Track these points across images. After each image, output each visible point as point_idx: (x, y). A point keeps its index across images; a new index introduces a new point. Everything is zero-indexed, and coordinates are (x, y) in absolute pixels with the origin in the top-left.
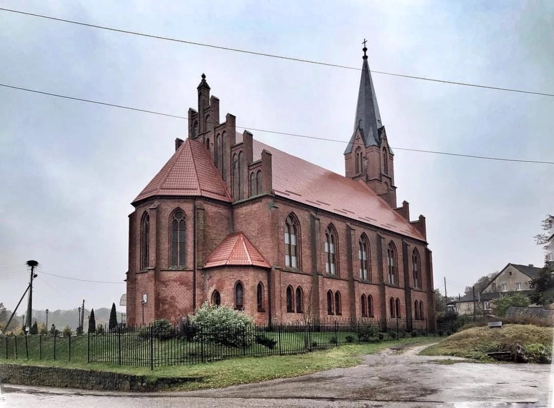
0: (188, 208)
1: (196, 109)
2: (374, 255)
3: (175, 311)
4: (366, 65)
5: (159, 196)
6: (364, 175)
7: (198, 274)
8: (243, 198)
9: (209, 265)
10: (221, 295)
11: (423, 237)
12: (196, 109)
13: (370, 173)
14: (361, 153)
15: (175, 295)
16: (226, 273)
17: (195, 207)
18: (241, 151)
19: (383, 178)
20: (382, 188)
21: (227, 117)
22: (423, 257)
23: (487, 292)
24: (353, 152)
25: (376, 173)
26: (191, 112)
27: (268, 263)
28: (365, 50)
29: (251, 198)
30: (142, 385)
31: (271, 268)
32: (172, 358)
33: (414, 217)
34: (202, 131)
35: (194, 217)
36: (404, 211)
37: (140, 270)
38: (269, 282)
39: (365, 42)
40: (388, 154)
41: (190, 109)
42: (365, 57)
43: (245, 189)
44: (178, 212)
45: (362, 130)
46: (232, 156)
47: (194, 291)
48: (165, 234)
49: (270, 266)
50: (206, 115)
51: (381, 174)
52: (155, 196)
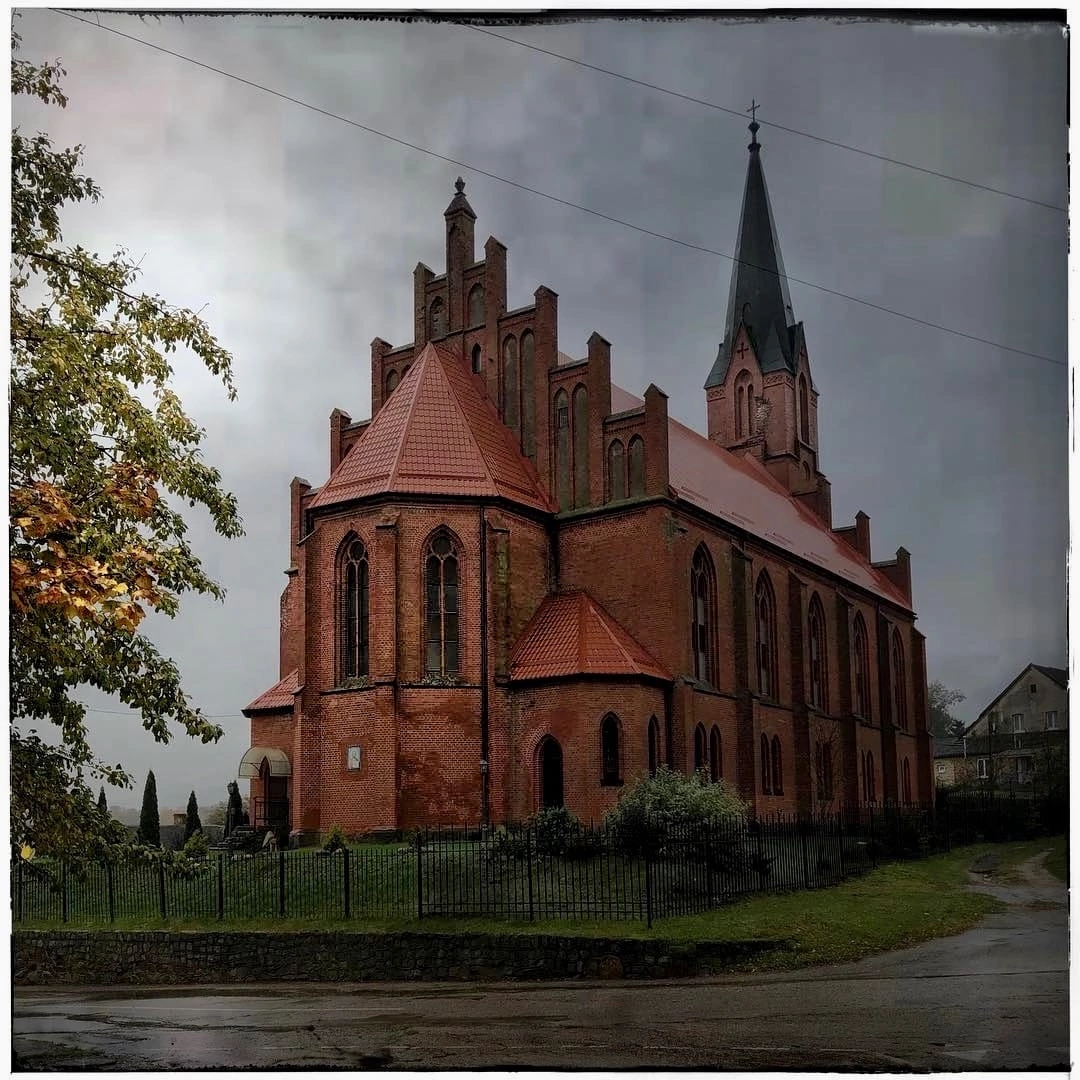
0: (465, 526)
1: (440, 270)
2: (832, 647)
3: (438, 789)
4: (755, 168)
5: (396, 494)
6: (756, 444)
7: (497, 696)
8: (589, 504)
9: (520, 675)
10: (563, 748)
11: (907, 601)
12: (440, 270)
13: (773, 439)
14: (751, 388)
15: (439, 751)
16: (581, 694)
17: (484, 524)
18: (580, 385)
19: (803, 452)
20: (797, 474)
21: (537, 294)
22: (908, 646)
23: (978, 733)
24: (731, 382)
25: (788, 440)
26: (423, 275)
27: (662, 667)
28: (754, 128)
29: (611, 505)
30: (656, 963)
31: (673, 683)
32: (547, 912)
33: (882, 551)
34: (458, 323)
35: (483, 550)
36: (855, 539)
37: (335, 686)
38: (669, 716)
39: (754, 109)
40: (809, 392)
41: (420, 264)
42: (754, 147)
43: (598, 481)
44: (442, 537)
45: (751, 327)
46: (552, 399)
47: (485, 737)
48: (413, 592)
49: (668, 674)
50: (471, 283)
51: (796, 441)
52: (388, 493)
